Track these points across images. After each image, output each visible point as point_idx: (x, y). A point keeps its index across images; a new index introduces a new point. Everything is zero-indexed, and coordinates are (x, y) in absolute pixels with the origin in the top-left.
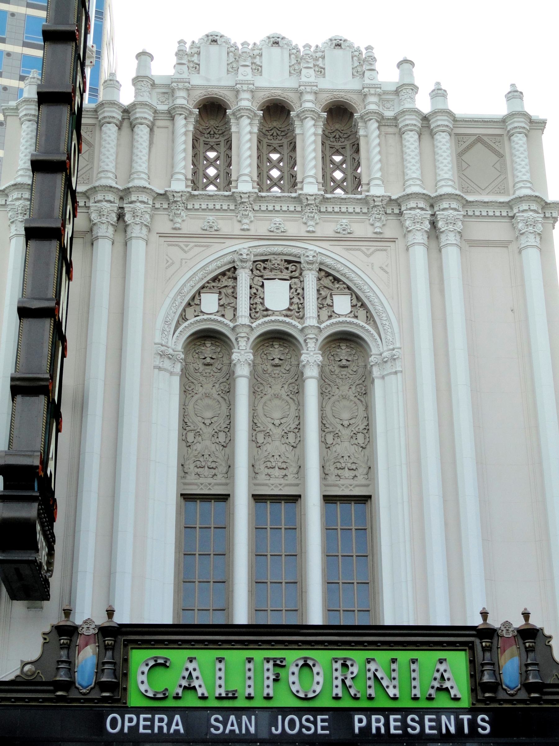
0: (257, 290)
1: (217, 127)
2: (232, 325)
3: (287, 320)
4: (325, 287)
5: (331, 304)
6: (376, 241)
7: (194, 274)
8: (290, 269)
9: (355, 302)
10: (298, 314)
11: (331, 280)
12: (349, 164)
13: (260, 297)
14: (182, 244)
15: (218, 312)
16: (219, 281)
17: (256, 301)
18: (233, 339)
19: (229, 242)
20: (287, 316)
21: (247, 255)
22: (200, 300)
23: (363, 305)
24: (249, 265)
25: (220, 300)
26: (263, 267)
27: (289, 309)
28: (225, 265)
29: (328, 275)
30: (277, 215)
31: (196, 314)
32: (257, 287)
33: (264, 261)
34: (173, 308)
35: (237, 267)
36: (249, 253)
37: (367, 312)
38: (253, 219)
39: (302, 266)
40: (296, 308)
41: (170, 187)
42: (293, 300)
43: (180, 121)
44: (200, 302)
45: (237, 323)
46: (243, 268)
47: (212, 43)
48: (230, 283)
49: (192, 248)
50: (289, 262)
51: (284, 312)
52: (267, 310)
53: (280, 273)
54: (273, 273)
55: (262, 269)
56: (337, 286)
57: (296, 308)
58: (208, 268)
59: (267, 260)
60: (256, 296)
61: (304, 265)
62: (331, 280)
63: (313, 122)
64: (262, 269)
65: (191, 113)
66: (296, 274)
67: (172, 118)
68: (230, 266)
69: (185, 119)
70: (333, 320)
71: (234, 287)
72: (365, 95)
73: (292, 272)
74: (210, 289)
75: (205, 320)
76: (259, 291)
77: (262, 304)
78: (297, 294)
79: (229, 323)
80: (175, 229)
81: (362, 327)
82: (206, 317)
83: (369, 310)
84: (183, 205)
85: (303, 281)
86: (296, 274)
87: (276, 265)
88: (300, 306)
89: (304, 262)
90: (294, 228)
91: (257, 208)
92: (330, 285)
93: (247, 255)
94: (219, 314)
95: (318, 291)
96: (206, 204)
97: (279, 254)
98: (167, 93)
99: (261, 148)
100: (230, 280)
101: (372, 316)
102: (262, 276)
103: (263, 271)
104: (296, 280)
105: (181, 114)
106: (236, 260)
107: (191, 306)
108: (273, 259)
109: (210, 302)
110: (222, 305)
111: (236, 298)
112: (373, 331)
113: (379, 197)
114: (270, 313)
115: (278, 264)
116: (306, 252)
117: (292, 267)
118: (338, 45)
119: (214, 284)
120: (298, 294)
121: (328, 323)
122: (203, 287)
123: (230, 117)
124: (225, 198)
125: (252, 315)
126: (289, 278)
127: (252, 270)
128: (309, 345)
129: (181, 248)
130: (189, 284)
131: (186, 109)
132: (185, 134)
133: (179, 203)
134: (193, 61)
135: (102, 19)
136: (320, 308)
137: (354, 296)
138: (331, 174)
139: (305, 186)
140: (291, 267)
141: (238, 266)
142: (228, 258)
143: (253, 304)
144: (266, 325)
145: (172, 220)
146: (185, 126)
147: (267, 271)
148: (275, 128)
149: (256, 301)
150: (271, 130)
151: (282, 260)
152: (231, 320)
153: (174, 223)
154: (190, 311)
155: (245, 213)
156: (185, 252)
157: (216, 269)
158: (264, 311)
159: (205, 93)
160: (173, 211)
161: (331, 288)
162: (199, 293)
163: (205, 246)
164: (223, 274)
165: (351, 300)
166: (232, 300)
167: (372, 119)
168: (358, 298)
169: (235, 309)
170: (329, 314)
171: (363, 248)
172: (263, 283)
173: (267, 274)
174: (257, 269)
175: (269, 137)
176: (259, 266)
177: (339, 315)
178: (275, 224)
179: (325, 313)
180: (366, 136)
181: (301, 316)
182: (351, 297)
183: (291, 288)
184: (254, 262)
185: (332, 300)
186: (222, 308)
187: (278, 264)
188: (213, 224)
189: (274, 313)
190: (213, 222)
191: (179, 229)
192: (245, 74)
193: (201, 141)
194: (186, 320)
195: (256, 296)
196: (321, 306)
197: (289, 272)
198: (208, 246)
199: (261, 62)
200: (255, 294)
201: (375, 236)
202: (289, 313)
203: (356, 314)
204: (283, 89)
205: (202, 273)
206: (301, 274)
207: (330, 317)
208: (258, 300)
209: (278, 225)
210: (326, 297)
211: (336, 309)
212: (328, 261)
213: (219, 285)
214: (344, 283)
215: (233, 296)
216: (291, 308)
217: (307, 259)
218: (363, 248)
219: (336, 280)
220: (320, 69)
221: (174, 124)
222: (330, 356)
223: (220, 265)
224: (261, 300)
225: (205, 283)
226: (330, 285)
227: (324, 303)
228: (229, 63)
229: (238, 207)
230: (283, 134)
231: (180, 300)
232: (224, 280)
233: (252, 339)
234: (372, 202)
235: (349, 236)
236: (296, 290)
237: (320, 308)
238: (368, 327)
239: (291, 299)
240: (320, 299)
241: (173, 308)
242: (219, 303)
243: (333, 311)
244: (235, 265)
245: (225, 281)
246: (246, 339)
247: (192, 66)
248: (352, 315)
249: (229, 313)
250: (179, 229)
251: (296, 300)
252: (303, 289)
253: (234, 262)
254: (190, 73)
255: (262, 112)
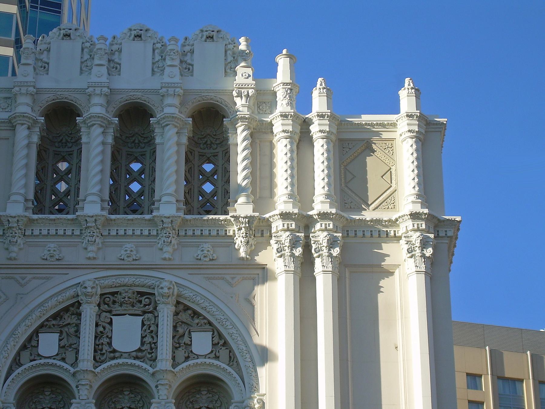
0: (104, 328)
1: (215, 135)
2: (72, 370)
3: (137, 362)
4: (182, 322)
5: (189, 343)
6: (66, 268)
7: (31, 311)
8: (143, 302)
9: (216, 340)
10: (150, 356)
11: (190, 315)
12: (220, 175)
13: (107, 336)
14: (228, 277)
15: (57, 355)
16: (61, 318)
17: (101, 341)
18: (74, 386)
19: (72, 273)
20: (136, 358)
21: (93, 288)
22: (38, 341)
23: (226, 344)
24: (97, 299)
25: (60, 340)
26: (112, 300)
27: (139, 350)
28: (68, 300)
29: (187, 308)
30: (51, 240)
31: (32, 358)
32: (104, 324)
33: (113, 294)
34: (4, 352)
35: (81, 302)
36: (95, 285)
37: (230, 352)
38: (22, 246)
39: (156, 299)
40: (147, 350)
41: (5, 211)
42: (144, 340)
43: (22, 132)
44: (38, 344)
45: (157, 369)
46: (88, 303)
47: (65, 38)
48: (74, 320)
49: (30, 281)
50: (142, 294)
51: (134, 354)
52: (114, 351)
53: (131, 308)
54: (123, 308)
55: (110, 303)
56: (197, 321)
57: (147, 350)
58: (47, 304)
59: (117, 293)
60: (102, 335)
61: (82, 297)
62: (190, 315)
63: (100, 130)
64: (110, 303)
65: (35, 122)
66: (151, 308)
67: (13, 128)
68: (75, 300)
69: (29, 128)
70: (191, 362)
71: (78, 326)
72: (90, 95)
73: (145, 305)
74: (50, 327)
75: (43, 365)
76: (107, 330)
77: (110, 344)
78: (150, 332)
79: (148, 367)
80: (10, 259)
81: (224, 370)
82: (42, 361)
83: (231, 348)
84: (20, 231)
85: (158, 316)
86: (151, 308)
87: (126, 299)
88: (153, 345)
89: (82, 294)
90: (148, 256)
91: (105, 233)
92: (189, 320)
93: (93, 288)
94: (59, 357)
95: (175, 327)
96: (47, 229)
97: (131, 286)
98: (10, 98)
99: (191, 158)
100: (73, 316)
101: (235, 356)
102: (110, 312)
103: (112, 306)
104: (150, 315)
105: (22, 124)
106: (80, 293)
107: (27, 349)
108: (123, 291)
109: (49, 343)
110: (64, 347)
111: (79, 338)
112: (235, 375)
113: (92, 217)
114: (117, 355)
115: (129, 298)
116: (161, 283)
117: (144, 302)
118: (67, 35)
119: (54, 322)
120: (152, 332)
121: (184, 365)
122: (42, 326)
123: (81, 125)
124: (70, 222)
125: (97, 358)
126: (141, 314)
127: (99, 305)
128: (160, 392)
129: (17, 281)
130: (24, 324)
131: (29, 118)
132: (28, 146)
133: (14, 229)
134: (41, 60)
135: (60, 13)
136: (176, 348)
137: (216, 333)
138: (200, 186)
139: (86, 206)
140: (145, 300)
141: (82, 300)
142: (71, 292)
143: (98, 345)
144: (113, 369)
145: (7, 249)
146: (29, 136)
147: (117, 305)
148: (137, 134)
149: (102, 341)
150: (203, 138)
151: (134, 293)
152: (72, 365)
153: (10, 253)
154: (25, 355)
155: (90, 239)
156: (22, 286)
157: (56, 305)
158: (111, 352)
159: (54, 98)
160: (9, 238)
161: (189, 323)
162: (36, 332)
163: (44, 278)
164: (66, 310)
165: (213, 338)
166: (73, 340)
167: (95, 124)
168: (220, 336)
169: (77, 353)
170: (186, 355)
171: (17, 276)
172: (111, 319)
173: (117, 309)
174: (105, 304)
175: (130, 145)
176: (108, 299)
177: (198, 356)
178: (49, 251)
179: (181, 354)
180: (88, 143)
181: (154, 357)
182: (213, 334)
183: (143, 324)
184: (102, 295)
185: (191, 338)
186: (62, 350)
187: (129, 298)
188: (55, 253)
189: (122, 355)
190: (54, 251)
191: (15, 259)
192: (99, 74)
193: (197, 154)
194: (20, 365)
195: (102, 335)
196: (178, 345)
197: (142, 306)
198: (48, 279)
199: (49, 59)
200: (101, 332)
201: (89, 262)
202: (140, 354)
203: (217, 354)
204: (143, 91)
205: (39, 310)
206: (155, 308)
207: (187, 358)
208: (105, 340)
209: (128, 252)
210: (184, 334)
211: (195, 349)
212: (187, 293)
213: (61, 323)
214: (205, 318)
215: (76, 336)
216: (143, 348)
217: (161, 290)
218: (15, 276)
219: (196, 314)
220: (44, 64)
221: (15, 135)
222: (188, 403)
223: (61, 300)
224: (108, 340)
225: (44, 321)
226: (189, 320)
227: (181, 341)
228: (83, 60)
229: (83, 232)
230: (146, 141)
231: (12, 343)
232: (66, 317)
233: (95, 387)
234: (6, 223)
235: (211, 263)
236: (150, 327)
237: (176, 348)
238: (229, 369)
239: (143, 338)
240: (177, 337)
241: (4, 352)
242: (59, 345)
243: (192, 351)
244: (79, 299)
245: (68, 319)
246: (88, 387)
247: (40, 65)
248: (213, 355)
249: (70, 356)
250: (15, 259)
251: (148, 339)
252: (157, 326)
253: (78, 296)
254: (37, 74)
255: (117, 119)
